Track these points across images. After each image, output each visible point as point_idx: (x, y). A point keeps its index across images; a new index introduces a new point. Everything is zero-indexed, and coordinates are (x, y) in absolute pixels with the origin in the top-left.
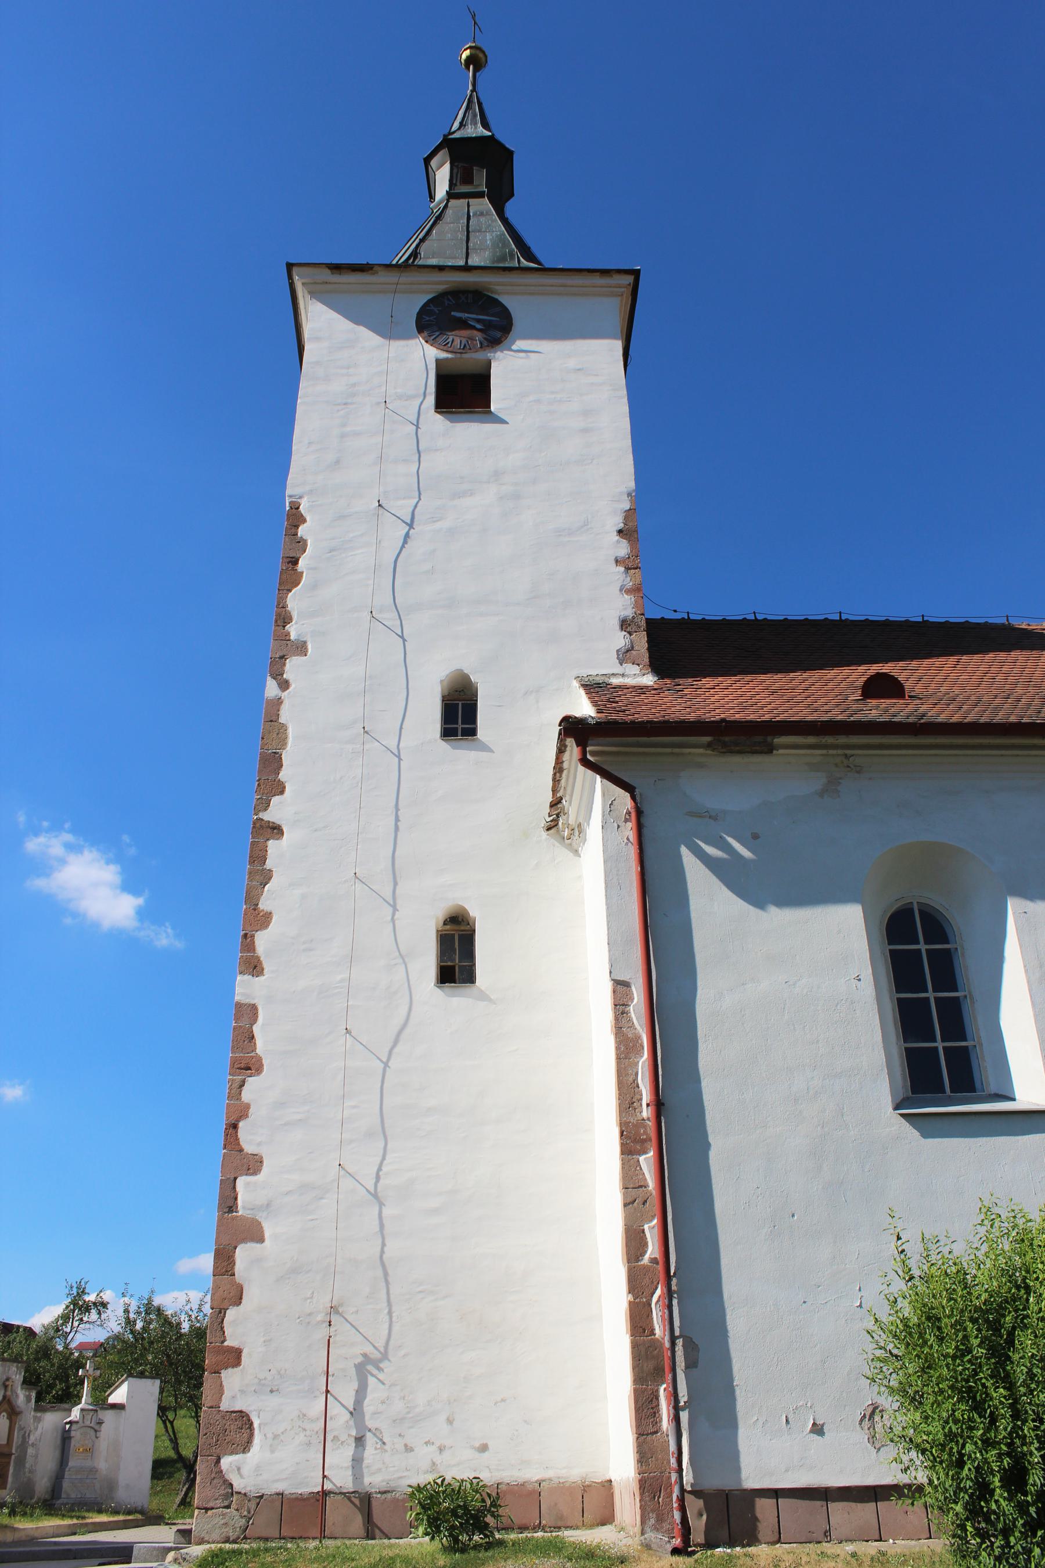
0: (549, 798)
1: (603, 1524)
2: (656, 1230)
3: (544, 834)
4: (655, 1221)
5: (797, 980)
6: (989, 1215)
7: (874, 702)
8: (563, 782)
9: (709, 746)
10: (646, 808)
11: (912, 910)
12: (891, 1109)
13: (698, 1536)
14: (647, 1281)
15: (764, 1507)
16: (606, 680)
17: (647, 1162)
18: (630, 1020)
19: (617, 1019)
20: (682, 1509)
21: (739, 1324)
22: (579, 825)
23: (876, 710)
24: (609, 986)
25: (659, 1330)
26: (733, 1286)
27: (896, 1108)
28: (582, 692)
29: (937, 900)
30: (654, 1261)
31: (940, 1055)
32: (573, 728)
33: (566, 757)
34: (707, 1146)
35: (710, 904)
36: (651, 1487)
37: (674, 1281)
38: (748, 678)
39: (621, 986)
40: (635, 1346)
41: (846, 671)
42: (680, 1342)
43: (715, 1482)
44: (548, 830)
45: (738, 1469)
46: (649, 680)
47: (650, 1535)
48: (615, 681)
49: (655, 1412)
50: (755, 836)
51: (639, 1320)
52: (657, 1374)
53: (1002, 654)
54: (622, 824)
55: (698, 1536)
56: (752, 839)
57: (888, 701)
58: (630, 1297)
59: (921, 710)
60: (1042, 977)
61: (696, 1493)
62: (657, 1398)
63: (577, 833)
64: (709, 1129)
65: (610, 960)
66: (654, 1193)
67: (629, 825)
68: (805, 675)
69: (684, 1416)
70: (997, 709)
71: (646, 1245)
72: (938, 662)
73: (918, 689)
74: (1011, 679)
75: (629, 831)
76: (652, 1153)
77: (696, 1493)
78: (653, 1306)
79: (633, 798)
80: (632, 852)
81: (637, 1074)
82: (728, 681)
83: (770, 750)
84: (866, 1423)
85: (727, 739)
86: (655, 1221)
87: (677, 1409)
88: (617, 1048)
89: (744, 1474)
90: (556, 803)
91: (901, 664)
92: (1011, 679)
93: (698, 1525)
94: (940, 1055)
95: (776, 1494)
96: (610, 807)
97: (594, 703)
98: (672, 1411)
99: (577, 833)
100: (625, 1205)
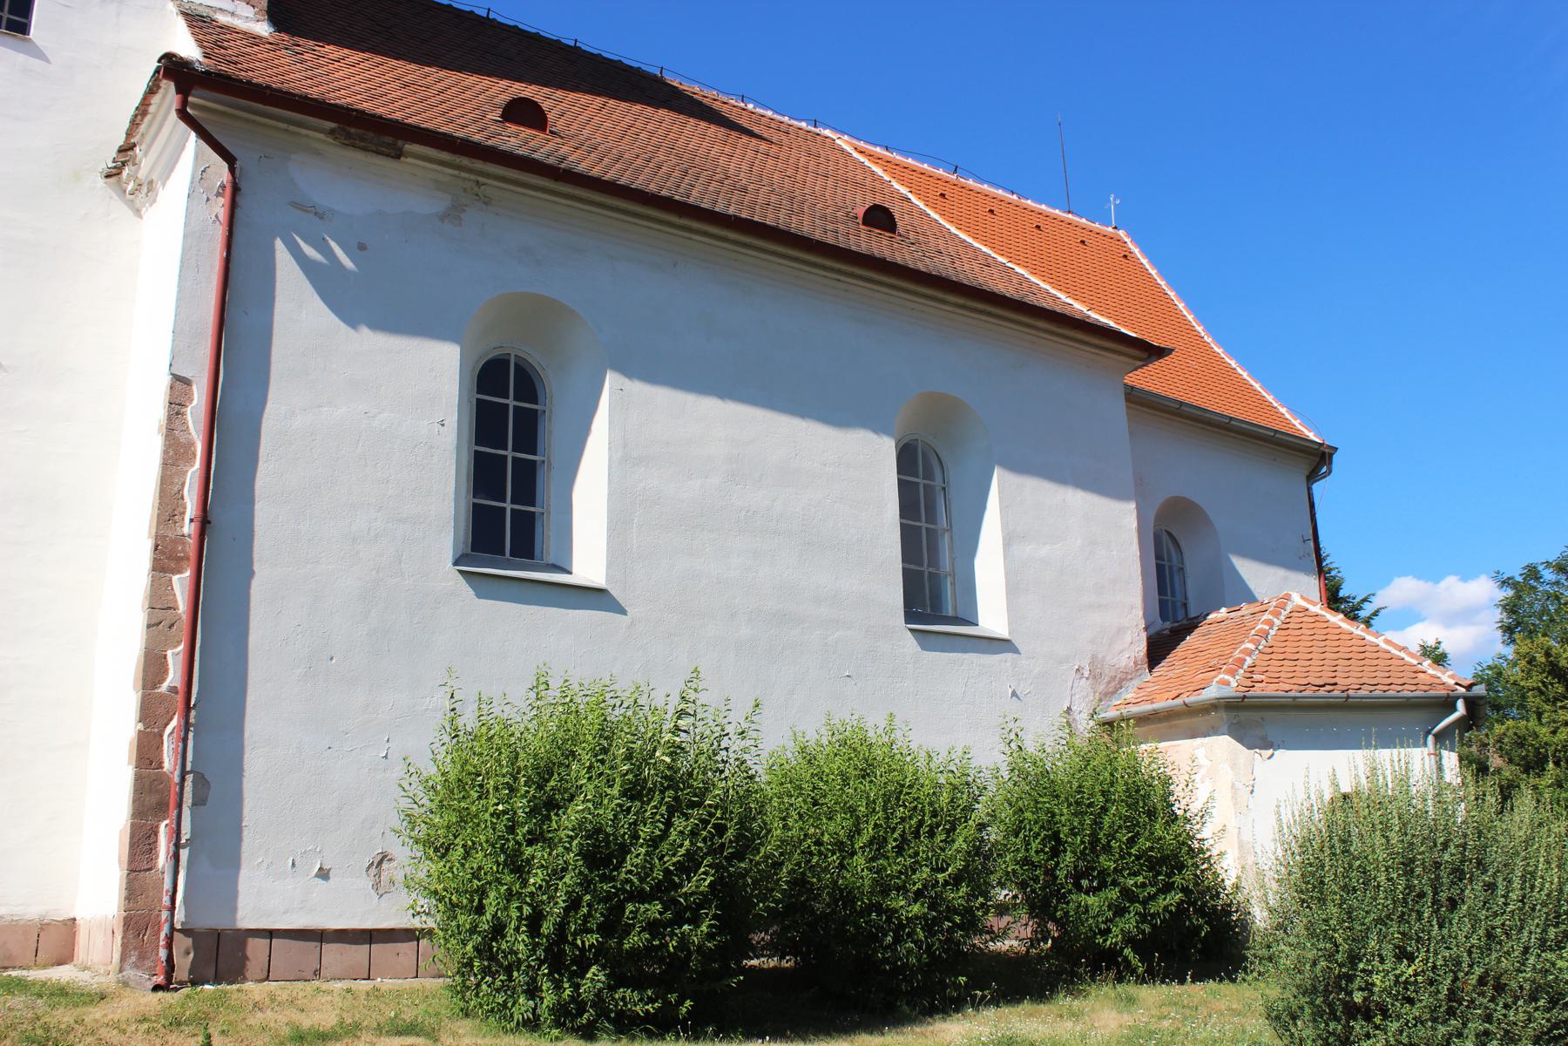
0: (121, 141)
1: (59, 964)
2: (181, 656)
3: (101, 182)
4: (181, 647)
5: (375, 410)
6: (541, 684)
7: (513, 128)
8: (143, 128)
9: (332, 132)
10: (243, 185)
11: (508, 362)
12: (450, 564)
13: (182, 973)
14: (161, 710)
15: (256, 947)
16: (211, 14)
17: (181, 584)
18: (185, 423)
19: (170, 419)
20: (169, 946)
21: (255, 763)
22: (151, 182)
23: (515, 139)
24: (166, 380)
25: (169, 762)
26: (256, 724)
27: (456, 563)
28: (181, 23)
29: (535, 358)
30: (173, 690)
31: (506, 516)
32: (172, 67)
33: (156, 99)
34: (251, 574)
35: (297, 311)
36: (136, 926)
37: (193, 713)
38: (378, 59)
39: (180, 382)
40: (138, 779)
41: (486, 81)
42: (190, 778)
43: (209, 920)
44: (108, 176)
45: (234, 909)
46: (263, 29)
47: (130, 973)
48: (222, 19)
49: (152, 849)
50: (362, 247)
51: (146, 752)
52: (161, 809)
53: (650, 109)
54: (213, 198)
55: (182, 973)
56: (359, 249)
57: (529, 131)
58: (140, 726)
59: (561, 152)
60: (624, 459)
61: (186, 932)
62: (156, 834)
63: (145, 189)
64: (256, 556)
65: (173, 351)
66: (184, 617)
67: (221, 201)
68: (443, 73)
69: (184, 854)
70: (638, 171)
71: (166, 671)
72: (585, 99)
73: (560, 126)
74: (654, 141)
75: (220, 207)
76: (188, 573)
77: (186, 932)
78: (165, 737)
79: (232, 170)
80: (219, 232)
81: (183, 484)
82: (356, 56)
83: (398, 155)
84: (373, 871)
85: (353, 130)
86: (181, 647)
87: (178, 846)
88: (165, 452)
89: (240, 914)
90: (127, 148)
91: (546, 90)
92: (654, 141)
93: (183, 964)
94: (506, 516)
95: (271, 934)
96: (201, 175)
97: (200, 43)
98: (172, 848)
99: (145, 189)
100: (149, 626)
